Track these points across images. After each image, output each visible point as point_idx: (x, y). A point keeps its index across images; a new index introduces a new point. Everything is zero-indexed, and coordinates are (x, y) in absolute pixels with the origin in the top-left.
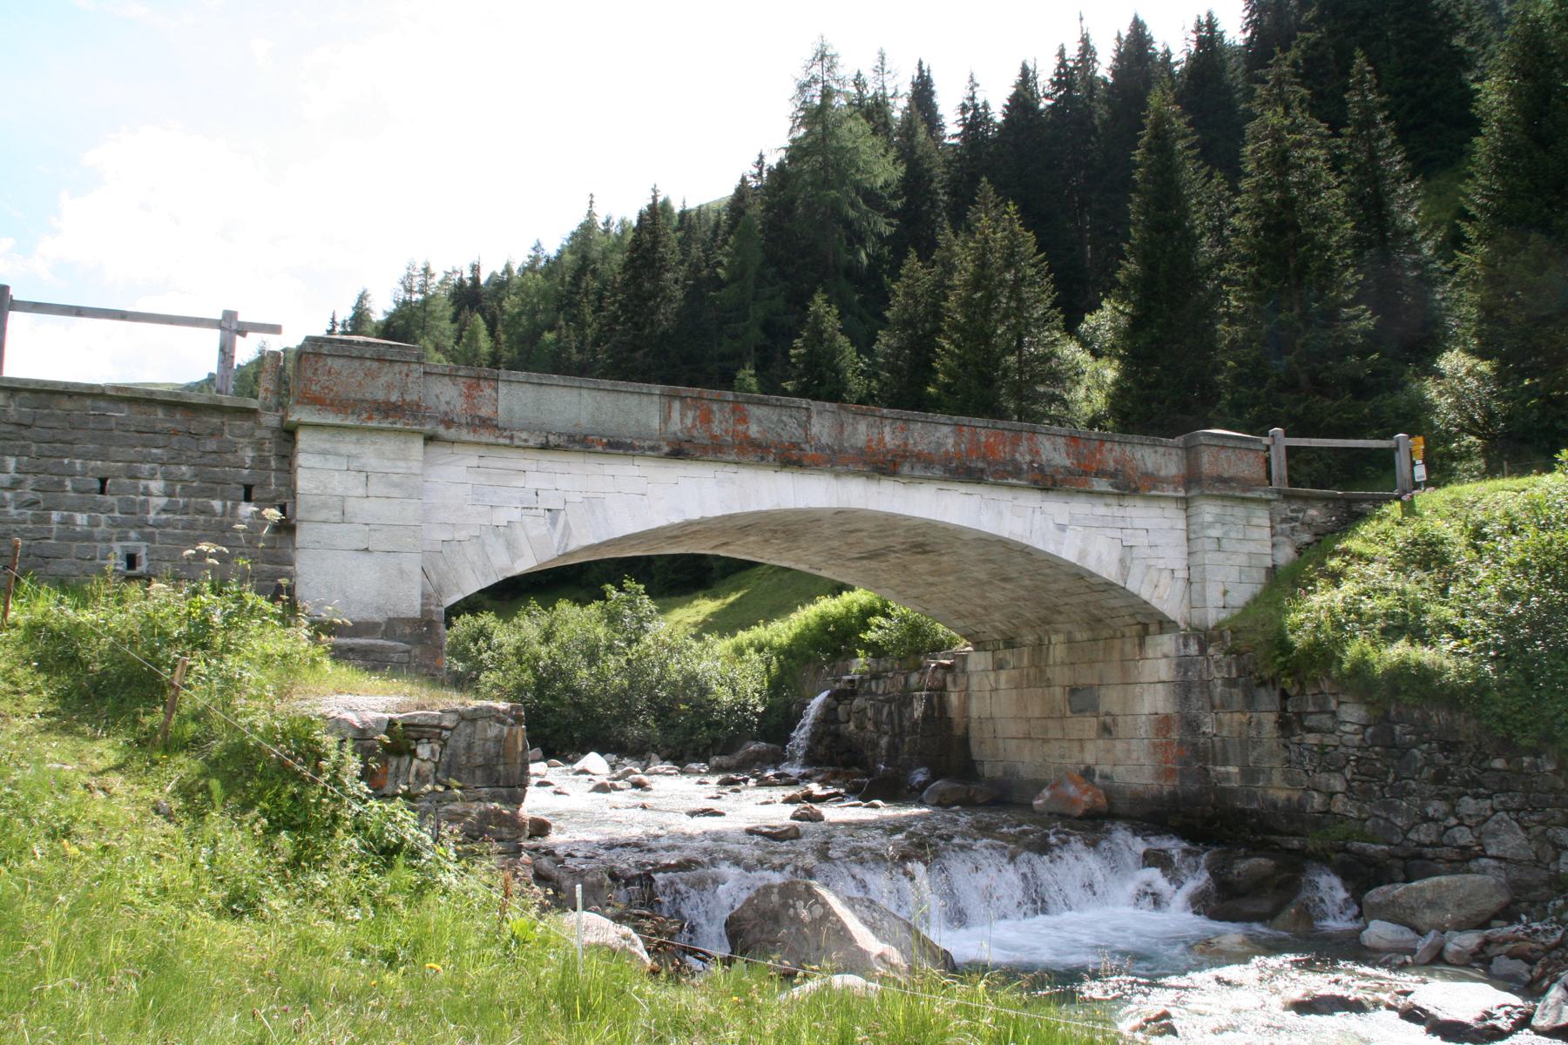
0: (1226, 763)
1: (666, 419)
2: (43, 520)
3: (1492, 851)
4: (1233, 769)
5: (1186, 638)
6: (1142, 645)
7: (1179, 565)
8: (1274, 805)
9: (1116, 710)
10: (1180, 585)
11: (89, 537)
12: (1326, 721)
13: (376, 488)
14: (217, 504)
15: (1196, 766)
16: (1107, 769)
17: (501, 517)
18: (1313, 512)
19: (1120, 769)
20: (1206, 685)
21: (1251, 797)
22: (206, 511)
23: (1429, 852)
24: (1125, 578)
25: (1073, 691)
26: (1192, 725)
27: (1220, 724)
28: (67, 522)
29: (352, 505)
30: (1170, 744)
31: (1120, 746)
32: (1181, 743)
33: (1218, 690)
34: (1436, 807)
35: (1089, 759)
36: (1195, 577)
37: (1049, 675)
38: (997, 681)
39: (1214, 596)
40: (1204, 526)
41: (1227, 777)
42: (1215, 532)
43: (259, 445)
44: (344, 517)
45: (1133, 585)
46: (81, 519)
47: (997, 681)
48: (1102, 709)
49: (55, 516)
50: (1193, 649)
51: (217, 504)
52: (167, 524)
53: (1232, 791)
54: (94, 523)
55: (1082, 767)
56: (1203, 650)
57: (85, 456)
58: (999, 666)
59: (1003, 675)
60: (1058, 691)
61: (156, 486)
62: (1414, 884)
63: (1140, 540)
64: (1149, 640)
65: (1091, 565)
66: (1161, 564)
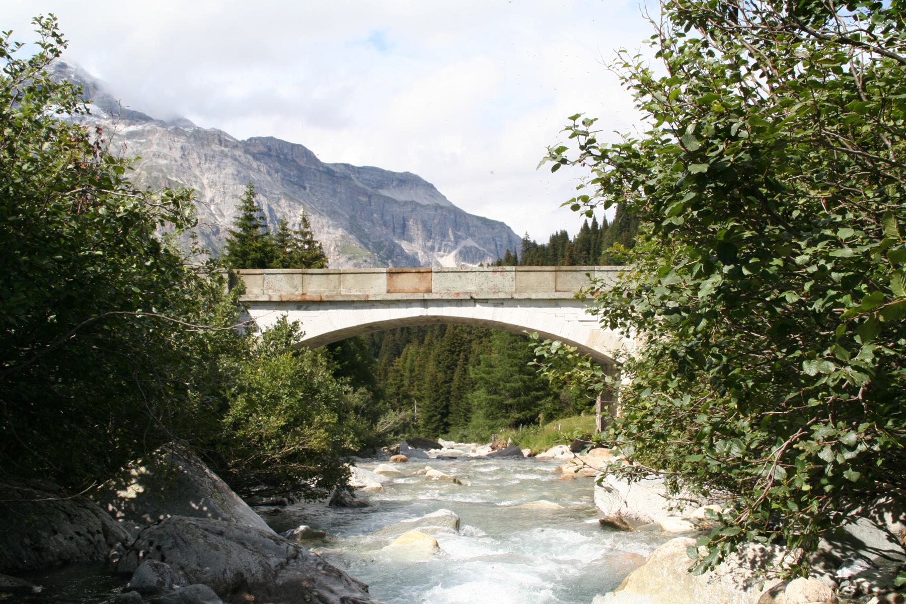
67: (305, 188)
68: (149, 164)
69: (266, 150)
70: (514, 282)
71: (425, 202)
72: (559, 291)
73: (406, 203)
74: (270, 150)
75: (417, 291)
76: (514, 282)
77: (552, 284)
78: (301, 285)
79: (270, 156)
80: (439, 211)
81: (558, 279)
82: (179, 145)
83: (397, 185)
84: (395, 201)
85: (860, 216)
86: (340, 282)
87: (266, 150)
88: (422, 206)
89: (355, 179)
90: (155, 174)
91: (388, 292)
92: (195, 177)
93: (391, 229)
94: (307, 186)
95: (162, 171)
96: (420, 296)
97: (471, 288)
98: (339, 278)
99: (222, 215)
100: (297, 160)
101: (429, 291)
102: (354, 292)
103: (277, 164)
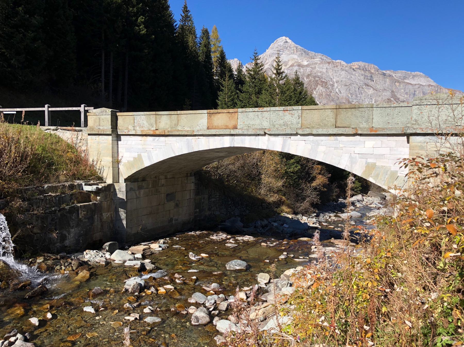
25: (168, 195)
55: (169, 219)
58: (140, 188)
59: (142, 191)
67: (373, 81)
68: (314, 75)
69: (358, 67)
70: (300, 119)
71: (424, 84)
72: (339, 127)
73: (416, 85)
74: (360, 67)
75: (227, 128)
76: (300, 119)
77: (333, 121)
78: (155, 123)
79: (360, 69)
80: (430, 87)
81: (338, 117)
82: (325, 67)
83: (412, 78)
84: (411, 84)
85: (425, 242)
86: (178, 121)
87: (358, 67)
88: (423, 85)
89: (394, 76)
90: (317, 79)
91: (208, 128)
92: (331, 79)
93: (409, 96)
94: (374, 80)
95: (319, 77)
96: (227, 132)
97: (266, 124)
98: (178, 117)
99: (341, 93)
100: (371, 70)
101: (235, 128)
102: (186, 129)
103: (363, 72)
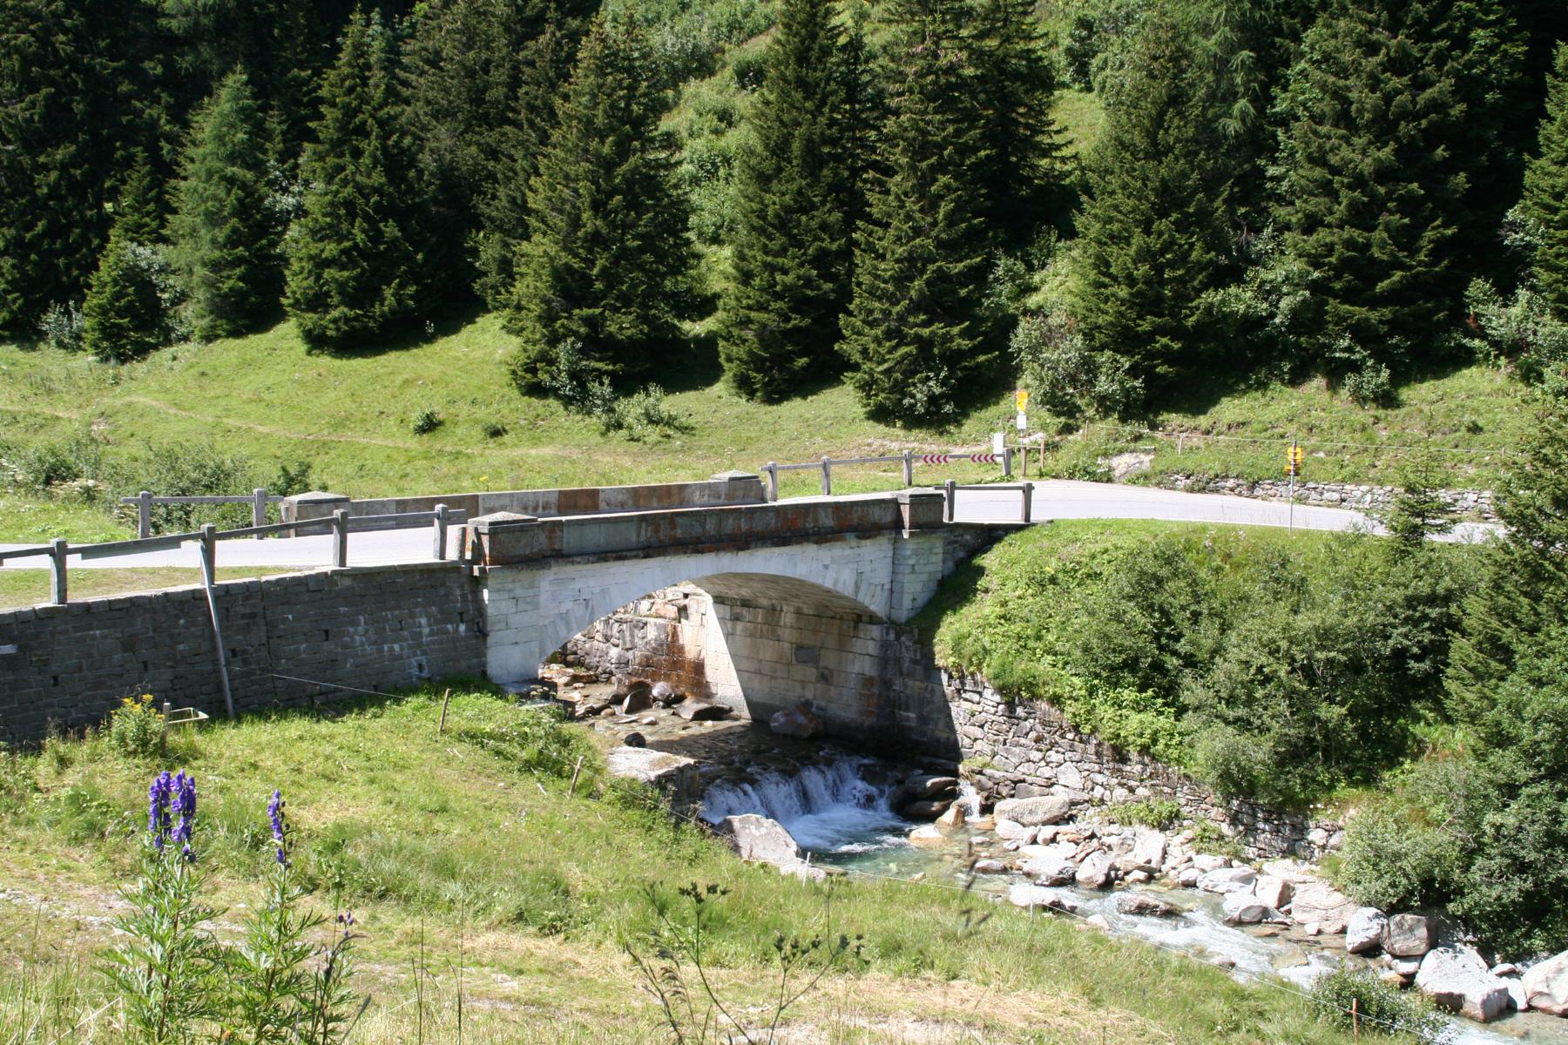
0: (907, 710)
1: (639, 535)
2: (381, 651)
3: (1062, 782)
4: (912, 715)
5: (888, 629)
6: (855, 627)
7: (886, 581)
8: (938, 741)
9: (832, 666)
10: (886, 593)
11: (401, 657)
12: (976, 697)
13: (522, 606)
14: (449, 627)
15: (888, 710)
16: (823, 704)
17: (563, 608)
18: (968, 537)
19: (832, 706)
20: (898, 661)
21: (923, 734)
22: (446, 632)
23: (1029, 779)
24: (857, 592)
26: (886, 684)
27: (905, 686)
28: (391, 649)
29: (511, 619)
30: (872, 695)
31: (833, 691)
32: (880, 695)
33: (906, 664)
34: (1035, 755)
35: (809, 695)
36: (896, 589)
37: (780, 631)
38: (734, 628)
39: (907, 602)
40: (905, 558)
41: (908, 719)
42: (911, 562)
43: (461, 587)
44: (507, 627)
45: (861, 598)
46: (396, 647)
47: (734, 628)
48: (822, 664)
49: (386, 648)
50: (892, 636)
51: (449, 627)
52: (433, 643)
53: (910, 728)
54: (402, 648)
56: (898, 637)
57: (391, 609)
58: (736, 618)
59: (740, 626)
60: (787, 645)
61: (423, 621)
62: (724, 476)
63: (866, 568)
64: (861, 626)
65: (840, 589)
66: (876, 581)
